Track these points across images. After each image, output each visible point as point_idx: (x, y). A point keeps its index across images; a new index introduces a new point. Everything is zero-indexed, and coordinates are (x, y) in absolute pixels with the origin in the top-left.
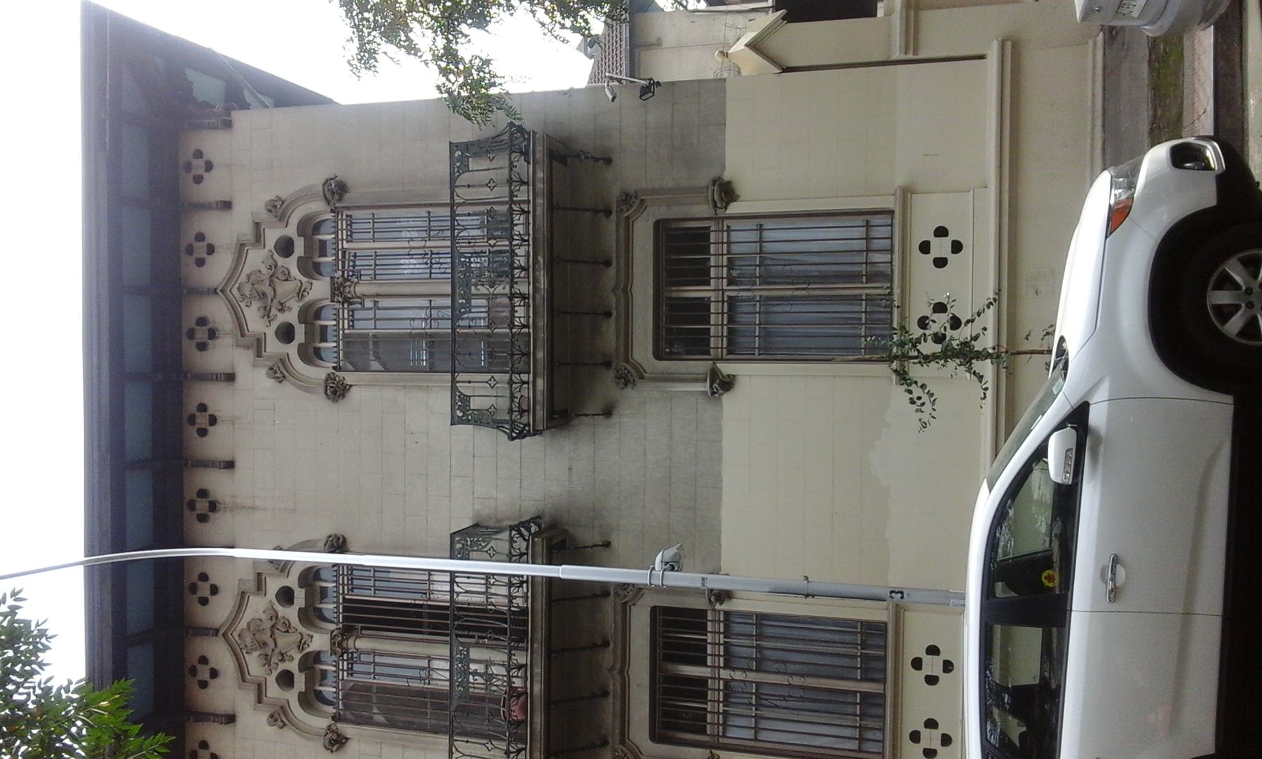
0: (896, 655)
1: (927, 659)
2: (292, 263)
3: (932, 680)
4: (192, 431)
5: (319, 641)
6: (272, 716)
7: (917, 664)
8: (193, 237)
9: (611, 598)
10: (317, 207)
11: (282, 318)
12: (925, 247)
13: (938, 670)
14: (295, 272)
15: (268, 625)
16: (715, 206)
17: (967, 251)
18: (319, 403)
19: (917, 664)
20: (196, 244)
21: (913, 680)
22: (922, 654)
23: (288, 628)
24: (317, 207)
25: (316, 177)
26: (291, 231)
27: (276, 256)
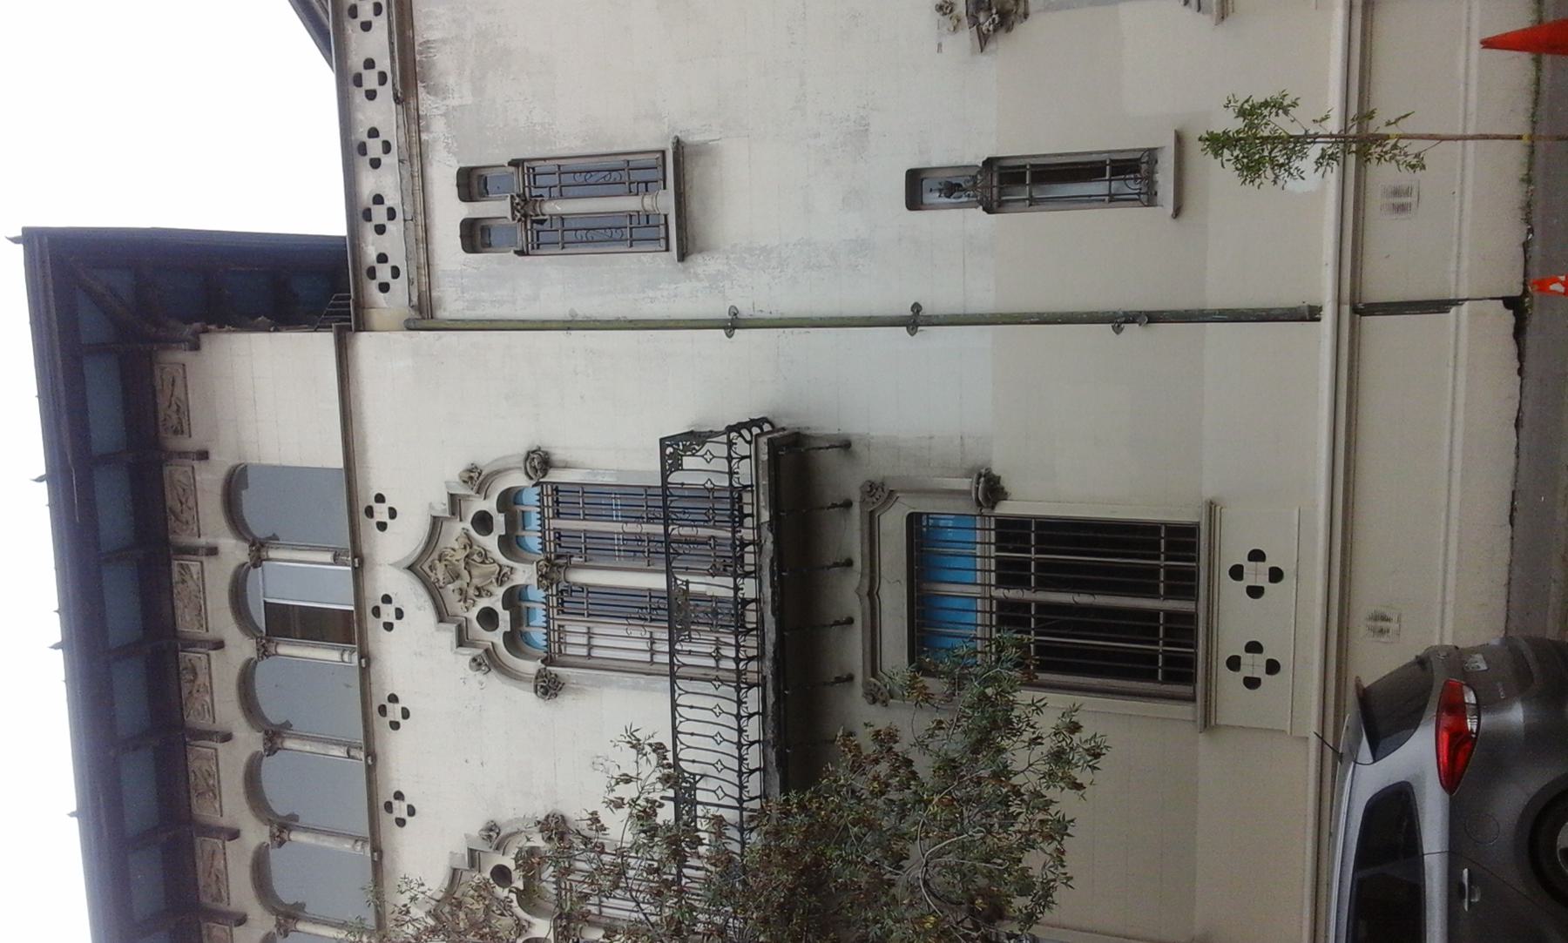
0: (1208, 653)
1: (1247, 658)
2: (490, 543)
3: (1255, 592)
4: (373, 287)
5: (525, 574)
6: (474, 660)
7: (1237, 573)
8: (374, 257)
9: (856, 509)
10: (518, 480)
11: (484, 603)
12: (1234, 663)
13: (1263, 580)
14: (496, 553)
15: (461, 555)
16: (979, 504)
17: (1288, 581)
18: (526, 697)
19: (1234, 663)
20: (389, 706)
21: (1231, 593)
22: (1242, 559)
23: (485, 556)
24: (518, 480)
25: (519, 447)
26: (490, 505)
27: (473, 533)
